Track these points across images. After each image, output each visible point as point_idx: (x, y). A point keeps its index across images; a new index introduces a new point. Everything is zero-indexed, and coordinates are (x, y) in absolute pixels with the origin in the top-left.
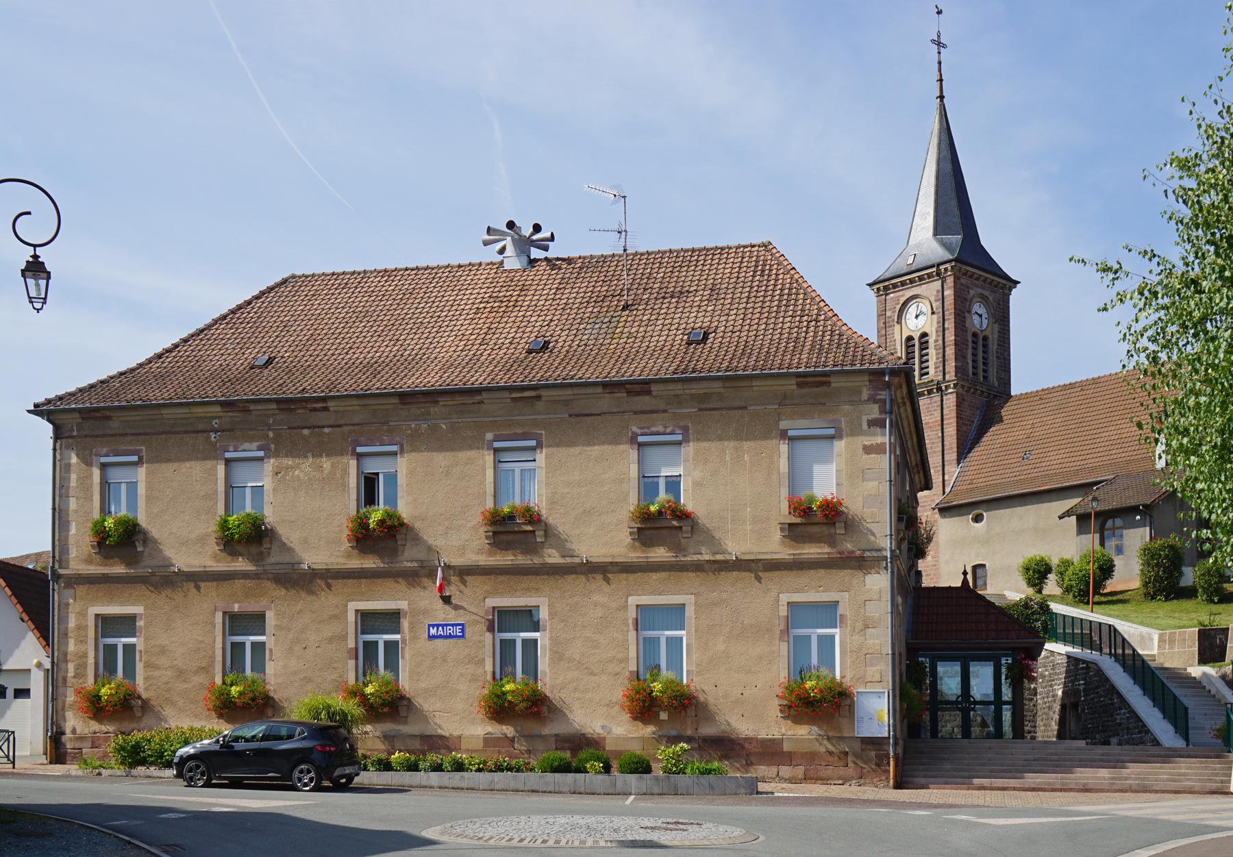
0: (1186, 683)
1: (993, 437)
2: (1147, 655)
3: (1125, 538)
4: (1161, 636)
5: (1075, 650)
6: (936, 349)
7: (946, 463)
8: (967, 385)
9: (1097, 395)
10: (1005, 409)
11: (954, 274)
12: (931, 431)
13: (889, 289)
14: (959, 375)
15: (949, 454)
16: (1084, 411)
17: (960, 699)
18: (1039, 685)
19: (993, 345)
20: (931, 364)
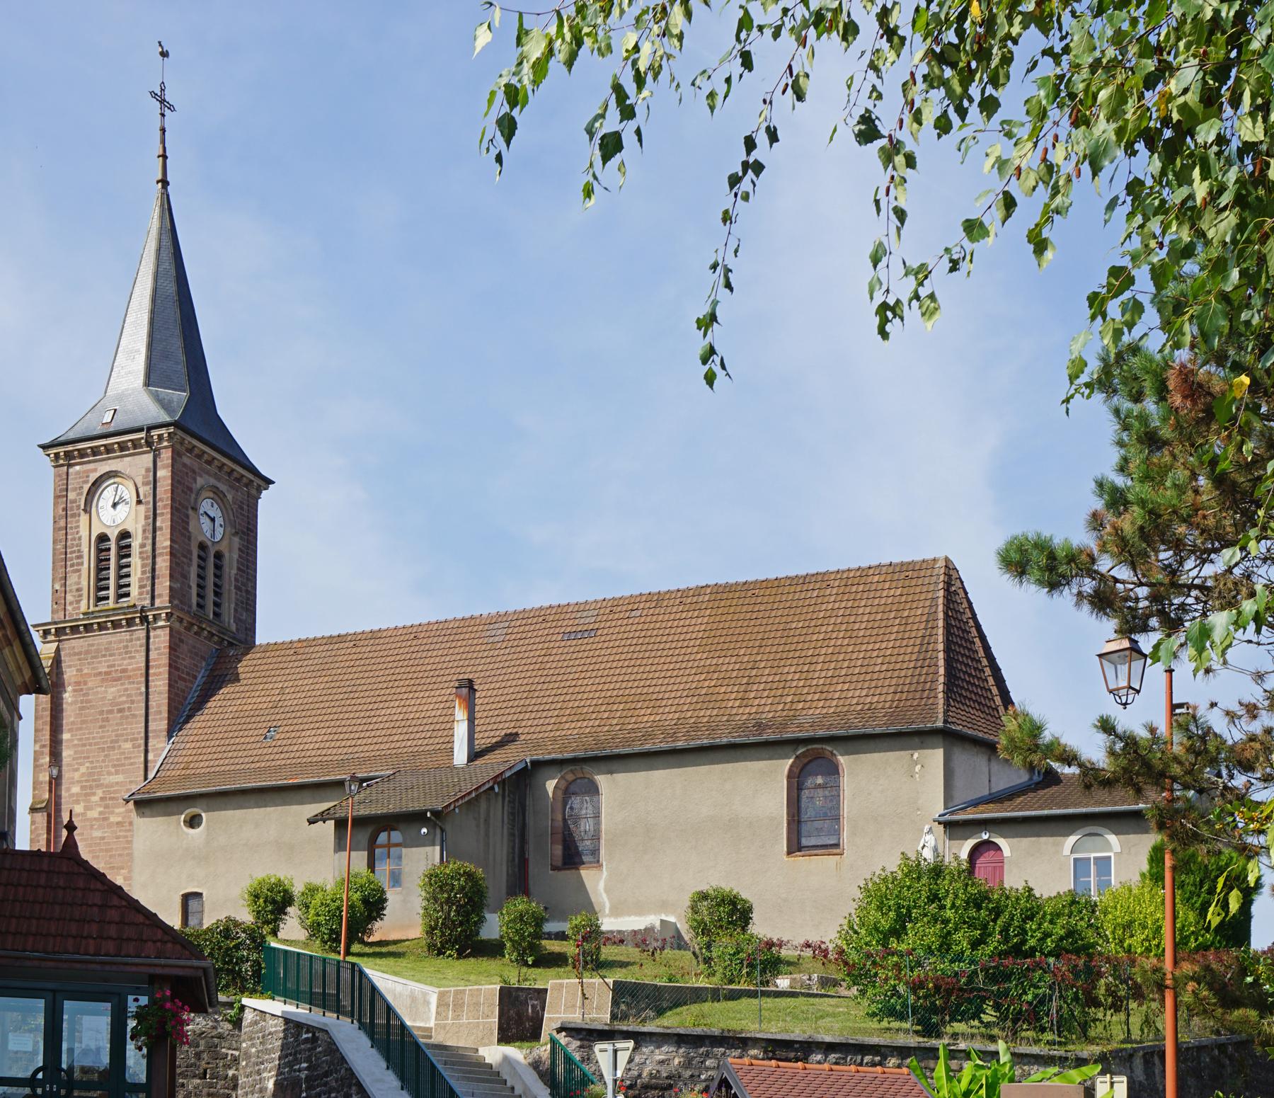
0: (479, 1073)
1: (223, 702)
2: (419, 1028)
3: (404, 861)
4: (442, 996)
5: (300, 1010)
6: (142, 558)
7: (150, 735)
8: (187, 618)
9: (376, 654)
10: (244, 663)
11: (172, 446)
12: (130, 683)
13: (74, 458)
14: (176, 602)
15: (155, 720)
16: (356, 676)
17: (40, 1076)
18: (241, 1071)
19: (231, 568)
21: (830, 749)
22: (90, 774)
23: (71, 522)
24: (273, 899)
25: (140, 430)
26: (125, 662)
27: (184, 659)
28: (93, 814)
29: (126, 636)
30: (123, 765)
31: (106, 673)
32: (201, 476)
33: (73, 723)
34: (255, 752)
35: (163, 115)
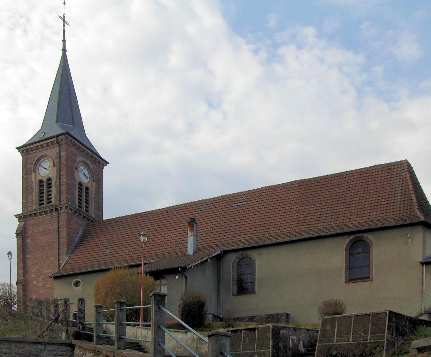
20: (53, 196)
21: (366, 235)
25: (54, 137)
26: (50, 227)
27: (73, 225)
28: (40, 284)
32: (79, 157)
35: (64, 26)
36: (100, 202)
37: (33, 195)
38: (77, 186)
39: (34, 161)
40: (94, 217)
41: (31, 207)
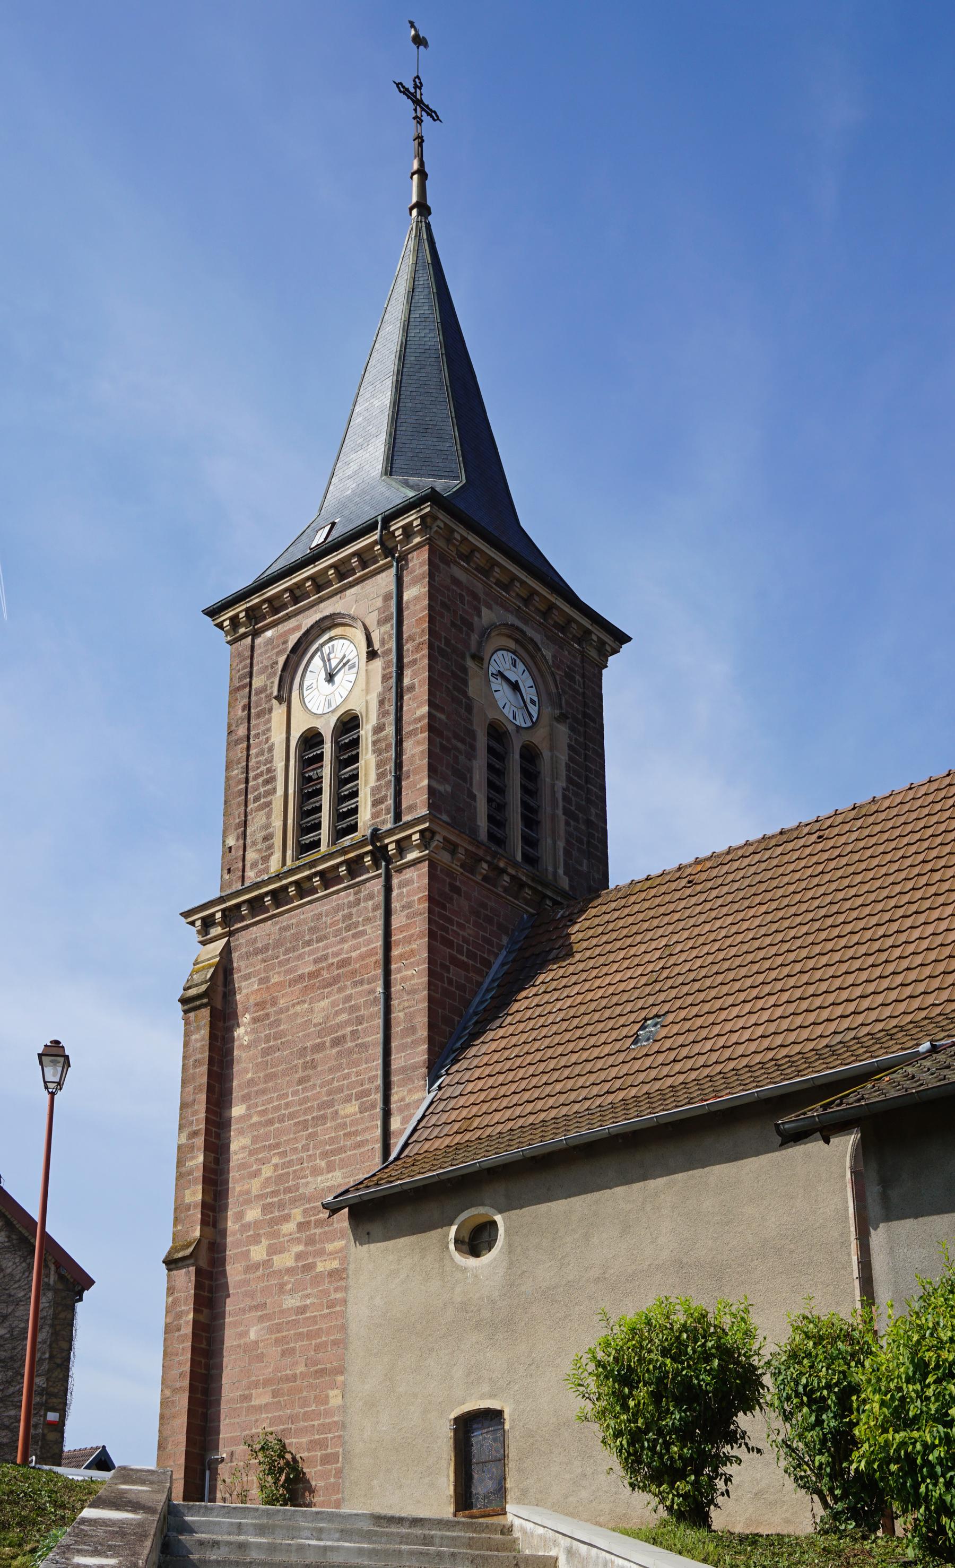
6: (378, 752)
7: (394, 1079)
8: (464, 844)
11: (430, 542)
12: (355, 984)
15: (404, 1047)
22: (280, 1179)
23: (257, 726)
24: (686, 1384)
25: (369, 528)
26: (345, 946)
29: (347, 897)
30: (342, 1150)
31: (313, 975)
32: (490, 607)
33: (251, 1082)
34: (613, 1072)
36: (593, 818)
37: (274, 806)
38: (482, 741)
39: (279, 653)
40: (567, 887)
41: (260, 867)
